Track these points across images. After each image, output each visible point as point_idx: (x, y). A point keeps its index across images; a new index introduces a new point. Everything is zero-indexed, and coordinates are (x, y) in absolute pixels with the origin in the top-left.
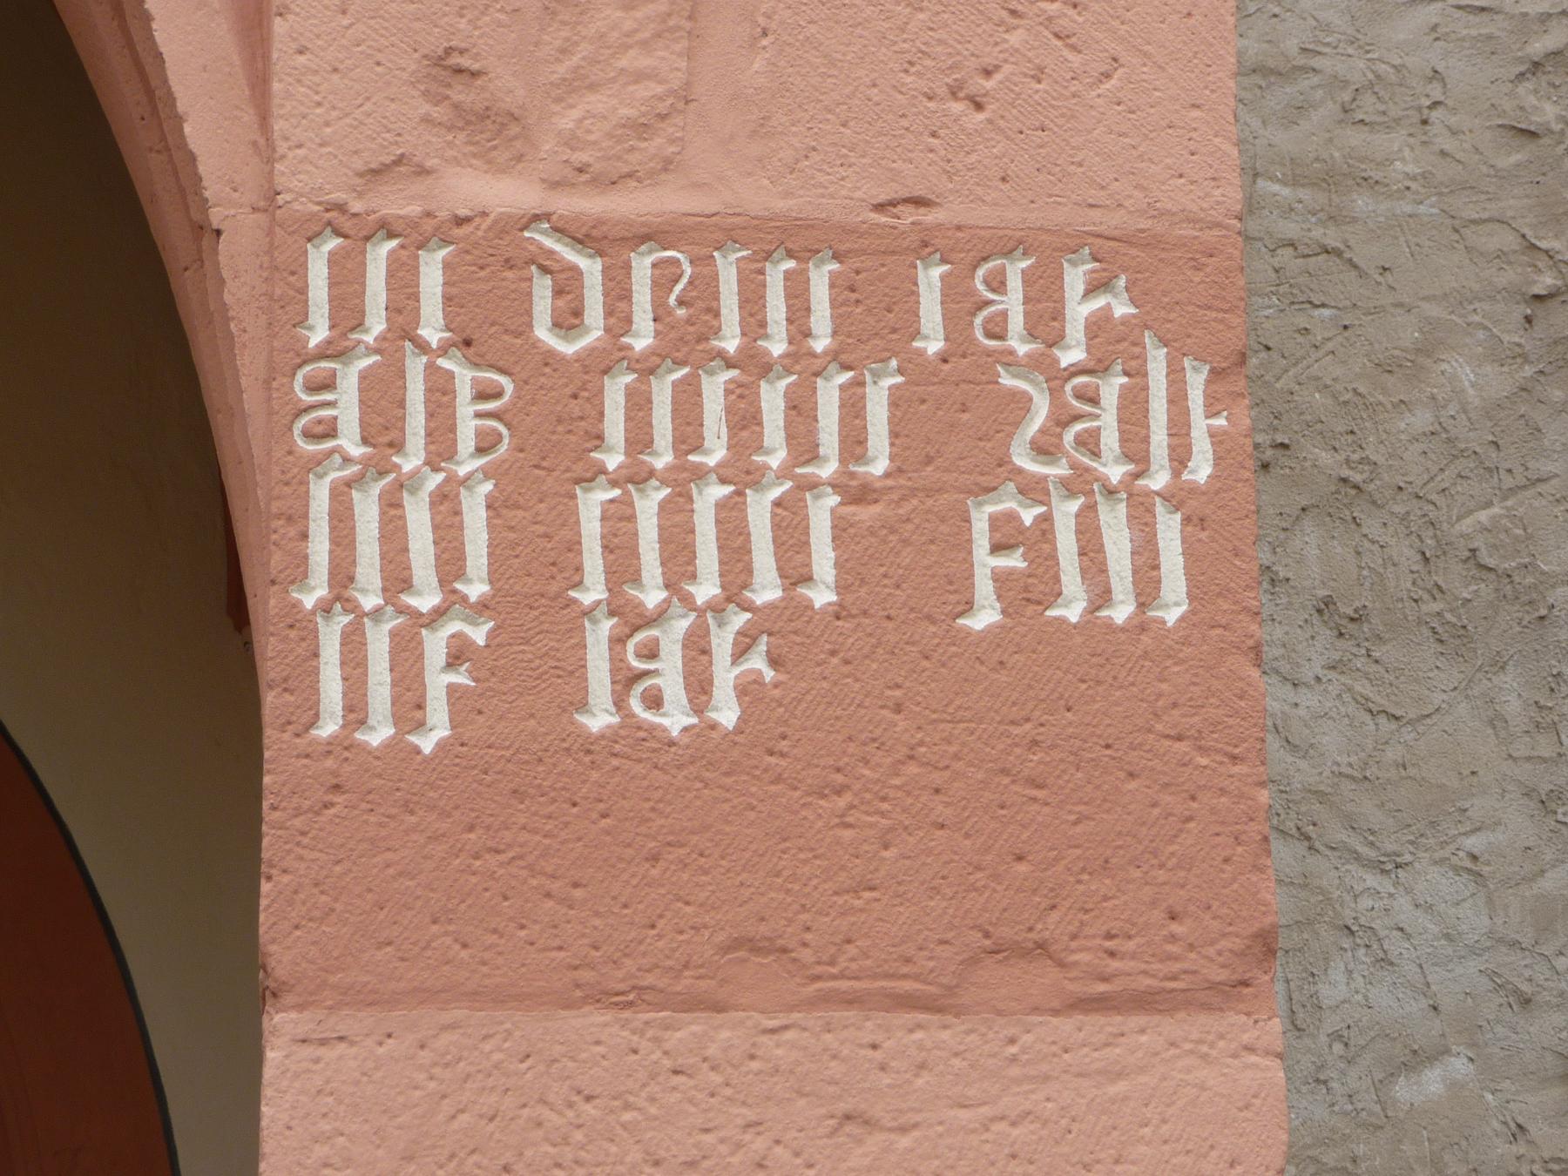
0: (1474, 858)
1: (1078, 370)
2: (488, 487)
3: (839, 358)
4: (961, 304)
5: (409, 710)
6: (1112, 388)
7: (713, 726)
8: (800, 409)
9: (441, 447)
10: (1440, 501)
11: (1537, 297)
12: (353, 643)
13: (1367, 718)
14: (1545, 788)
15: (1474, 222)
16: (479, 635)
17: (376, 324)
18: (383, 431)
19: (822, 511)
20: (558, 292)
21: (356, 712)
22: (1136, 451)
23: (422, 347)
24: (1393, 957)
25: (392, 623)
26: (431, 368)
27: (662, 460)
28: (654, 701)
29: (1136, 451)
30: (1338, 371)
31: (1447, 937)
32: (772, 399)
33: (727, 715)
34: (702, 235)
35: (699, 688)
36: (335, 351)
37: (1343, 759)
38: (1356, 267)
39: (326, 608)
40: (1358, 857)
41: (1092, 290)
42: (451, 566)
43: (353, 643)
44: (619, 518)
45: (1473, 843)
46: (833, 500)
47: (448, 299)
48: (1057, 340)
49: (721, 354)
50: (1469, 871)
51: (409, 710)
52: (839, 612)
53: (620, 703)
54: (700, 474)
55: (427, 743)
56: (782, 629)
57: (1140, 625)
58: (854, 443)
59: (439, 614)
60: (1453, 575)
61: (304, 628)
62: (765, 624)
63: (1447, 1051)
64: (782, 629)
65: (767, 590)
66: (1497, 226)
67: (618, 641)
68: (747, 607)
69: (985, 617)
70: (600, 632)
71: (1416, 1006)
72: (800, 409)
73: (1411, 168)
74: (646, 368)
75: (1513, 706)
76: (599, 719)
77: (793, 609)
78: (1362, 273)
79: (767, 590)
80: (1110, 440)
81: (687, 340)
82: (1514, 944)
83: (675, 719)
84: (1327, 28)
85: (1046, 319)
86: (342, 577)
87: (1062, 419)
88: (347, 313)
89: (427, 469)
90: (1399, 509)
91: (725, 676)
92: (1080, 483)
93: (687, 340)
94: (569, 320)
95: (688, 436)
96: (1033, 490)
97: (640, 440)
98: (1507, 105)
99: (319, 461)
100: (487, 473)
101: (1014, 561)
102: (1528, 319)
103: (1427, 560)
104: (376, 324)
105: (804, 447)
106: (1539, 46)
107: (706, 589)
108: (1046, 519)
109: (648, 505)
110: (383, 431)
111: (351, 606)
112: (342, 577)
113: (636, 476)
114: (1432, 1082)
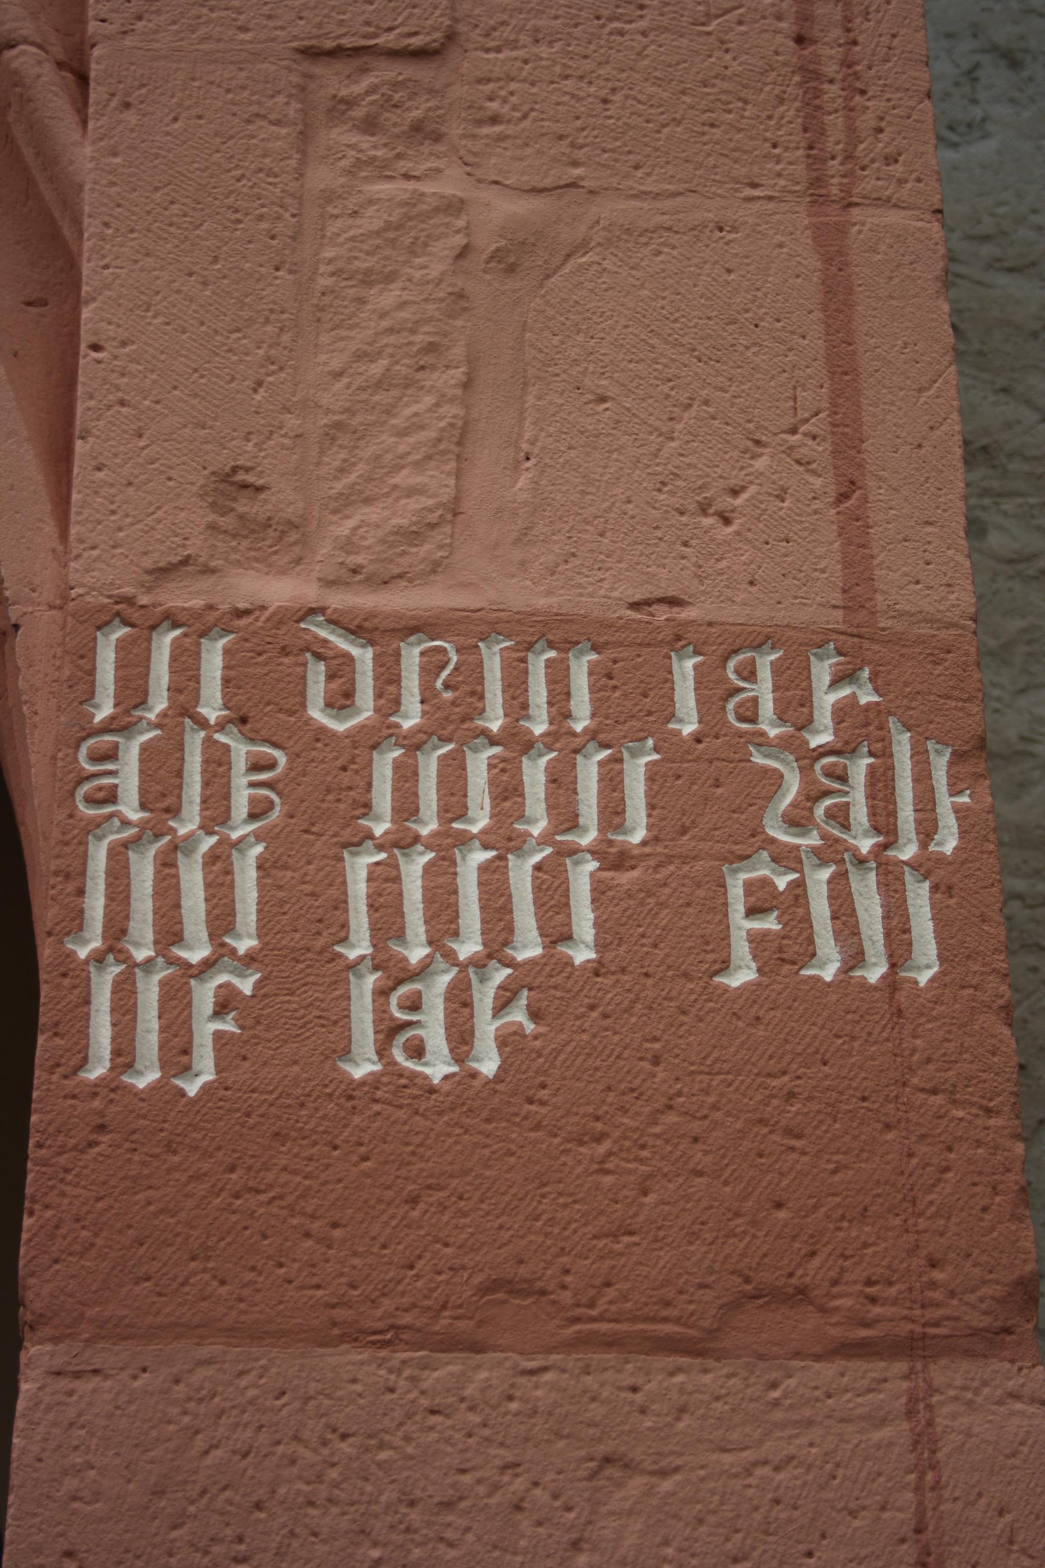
4: (713, 692)
5: (177, 1054)
6: (860, 768)
17: (159, 703)
18: (161, 796)
19: (582, 875)
21: (124, 1055)
22: (884, 823)
23: (202, 723)
26: (209, 743)
28: (417, 1051)
29: (884, 823)
32: (535, 773)
34: (471, 628)
35: (461, 1039)
39: (98, 959)
42: (221, 920)
44: (386, 883)
46: (592, 865)
48: (806, 723)
49: (485, 732)
51: (177, 1054)
52: (597, 969)
53: (382, 1051)
54: (463, 840)
56: (544, 984)
58: (613, 812)
59: (208, 965)
61: (78, 978)
62: (523, 980)
64: (544, 984)
65: (529, 947)
69: (742, 975)
74: (414, 744)
76: (363, 1068)
79: (529, 947)
80: (860, 814)
81: (454, 718)
83: (438, 1068)
85: (796, 706)
86: (117, 930)
87: (812, 795)
88: (133, 692)
91: (487, 1029)
93: (454, 718)
94: (342, 700)
96: (786, 857)
99: (97, 823)
100: (258, 837)
101: (770, 924)
104: (159, 703)
108: (799, 886)
109: (414, 869)
110: (161, 796)
112: (117, 930)
113: (403, 841)
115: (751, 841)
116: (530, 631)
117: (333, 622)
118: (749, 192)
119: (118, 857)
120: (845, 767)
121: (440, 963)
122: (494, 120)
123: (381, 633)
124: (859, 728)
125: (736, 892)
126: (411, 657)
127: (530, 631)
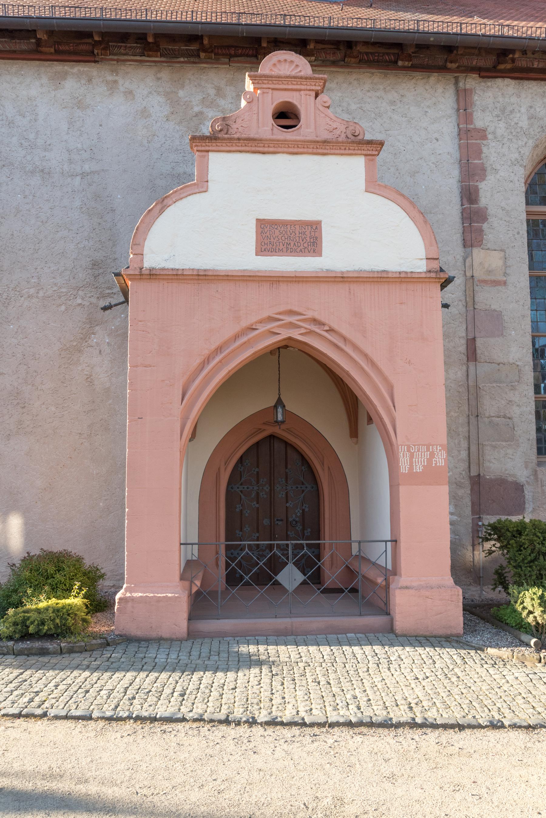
4: (432, 448)
8: (424, 454)
32: (423, 454)
34: (419, 445)
56: (424, 466)
62: (423, 466)
64: (424, 466)
69: (434, 465)
72: (424, 454)
75: (456, 443)
76: (415, 471)
81: (418, 451)
83: (418, 471)
85: (437, 449)
88: (402, 450)
89: (64, 651)
93: (418, 451)
115: (434, 457)
116: (422, 445)
120: (313, 74)
123: (414, 446)
124: (440, 450)
127: (422, 445)
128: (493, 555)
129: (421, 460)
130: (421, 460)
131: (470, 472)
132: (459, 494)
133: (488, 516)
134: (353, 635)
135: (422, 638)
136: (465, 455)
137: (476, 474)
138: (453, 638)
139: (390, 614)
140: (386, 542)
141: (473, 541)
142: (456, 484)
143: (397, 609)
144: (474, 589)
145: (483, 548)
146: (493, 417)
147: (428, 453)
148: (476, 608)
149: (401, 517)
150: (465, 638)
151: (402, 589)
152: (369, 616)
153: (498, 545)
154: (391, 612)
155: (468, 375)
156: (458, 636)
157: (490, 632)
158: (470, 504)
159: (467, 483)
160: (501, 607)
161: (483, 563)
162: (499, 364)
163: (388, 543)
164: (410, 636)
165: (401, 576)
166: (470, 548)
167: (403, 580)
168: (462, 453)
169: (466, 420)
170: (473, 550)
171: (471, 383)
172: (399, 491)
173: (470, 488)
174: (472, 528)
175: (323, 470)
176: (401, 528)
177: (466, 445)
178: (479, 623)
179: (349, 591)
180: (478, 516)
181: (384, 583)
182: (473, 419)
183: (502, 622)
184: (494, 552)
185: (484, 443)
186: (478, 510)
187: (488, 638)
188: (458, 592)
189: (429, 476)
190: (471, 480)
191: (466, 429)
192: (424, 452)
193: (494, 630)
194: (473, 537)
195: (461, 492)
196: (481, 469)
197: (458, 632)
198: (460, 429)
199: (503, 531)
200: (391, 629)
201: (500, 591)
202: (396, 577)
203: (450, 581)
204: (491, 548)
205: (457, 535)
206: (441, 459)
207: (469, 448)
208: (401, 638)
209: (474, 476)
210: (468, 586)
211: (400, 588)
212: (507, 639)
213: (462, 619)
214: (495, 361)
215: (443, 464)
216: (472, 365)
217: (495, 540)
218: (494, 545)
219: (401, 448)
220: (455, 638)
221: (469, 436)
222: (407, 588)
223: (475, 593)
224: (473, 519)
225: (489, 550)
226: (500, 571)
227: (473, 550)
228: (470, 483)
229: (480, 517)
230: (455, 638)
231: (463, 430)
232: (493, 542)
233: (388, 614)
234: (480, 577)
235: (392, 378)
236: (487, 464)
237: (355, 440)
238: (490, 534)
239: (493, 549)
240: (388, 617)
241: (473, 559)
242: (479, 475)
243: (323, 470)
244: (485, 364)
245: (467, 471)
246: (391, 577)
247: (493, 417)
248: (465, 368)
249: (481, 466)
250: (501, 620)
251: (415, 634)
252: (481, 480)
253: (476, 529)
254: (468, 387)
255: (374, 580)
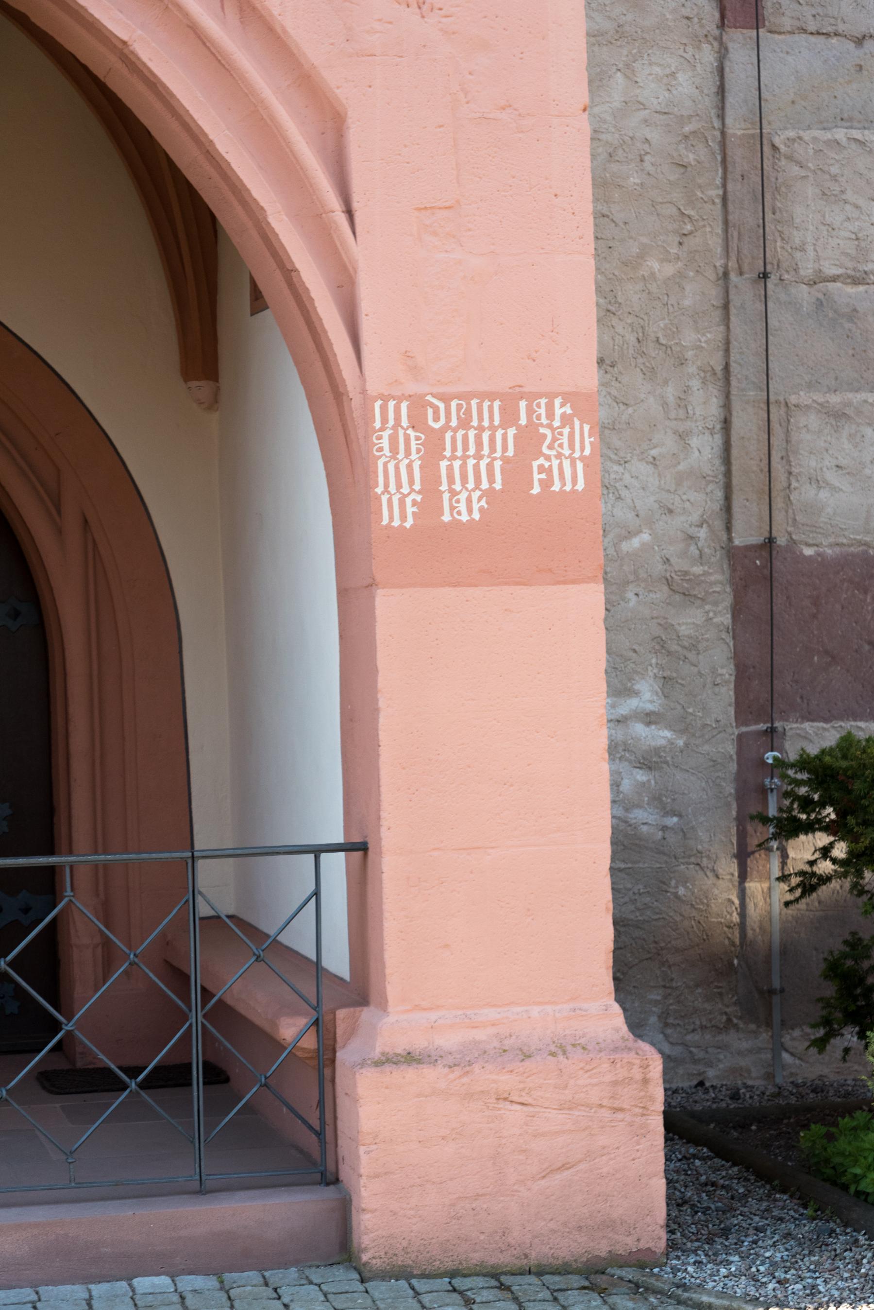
0: (654, 458)
1: (558, 428)
2: (420, 462)
3: (500, 426)
4: (530, 411)
5: (403, 517)
6: (566, 431)
7: (474, 520)
8: (492, 440)
9: (408, 453)
10: (646, 318)
11: (685, 235)
12: (390, 501)
13: (615, 404)
14: (681, 430)
15: (661, 203)
16: (419, 498)
17: (391, 422)
18: (394, 450)
19: (498, 464)
20: (434, 413)
21: (391, 518)
22: (572, 446)
23: (402, 428)
24: (623, 496)
25: (398, 496)
26: (405, 434)
27: (459, 453)
28: (459, 513)
29: (572, 446)
30: (607, 266)
31: (643, 489)
32: (485, 436)
33: (476, 516)
34: (466, 397)
35: (470, 511)
36: (383, 429)
37: (606, 421)
38: (614, 222)
39: (383, 493)
40: (610, 459)
41: (562, 405)
42: (411, 482)
43: (390, 501)
44: (450, 468)
45: (654, 452)
46: (501, 463)
47: (409, 416)
48: (553, 420)
49: (473, 427)
50: (652, 463)
51: (403, 517)
52: (502, 491)
53: (452, 515)
54: (469, 457)
55: (408, 525)
56: (489, 494)
57: (573, 491)
58: (505, 448)
59: (409, 494)
60: (651, 350)
61: (378, 498)
62: (485, 494)
63: (641, 532)
64: (489, 494)
65: (485, 485)
66: (669, 205)
67: (450, 500)
68: (481, 490)
69: (536, 490)
70: (446, 496)
71: (631, 515)
72: (492, 440)
73: (638, 181)
74: (455, 430)
75: (671, 399)
76: (447, 518)
77: (491, 490)
78: (617, 225)
79: (485, 485)
80: (566, 445)
81: (465, 423)
82: (669, 491)
83: (465, 518)
84: (605, 122)
85: (550, 415)
86: (386, 485)
87: (554, 440)
88: (384, 420)
90: (629, 321)
91: (475, 507)
92: (559, 456)
93: (465, 423)
94: (436, 419)
95: (466, 448)
96: (548, 458)
97: (454, 449)
98: (675, 154)
99: (380, 457)
100: (419, 458)
101: (543, 476)
102: (680, 243)
103: (639, 342)
104: (391, 422)
105: (493, 449)
106: (687, 129)
107: (471, 485)
108: (551, 466)
109: (457, 464)
110: (394, 450)
111: (389, 493)
112: (386, 485)
113: (453, 458)
114: (636, 542)
116: (482, 396)
117: (434, 396)
118: (542, 251)
119: (385, 465)
121: (464, 490)
122: (470, 230)
123: (446, 399)
124: (566, 420)
125: (535, 469)
126: (454, 404)
127: (482, 396)
128: (824, 891)
129: (476, 467)
130: (476, 467)
131: (729, 529)
132: (684, 630)
133: (807, 725)
134: (163, 1281)
135: (480, 1282)
136: (707, 453)
137: (756, 539)
138: (618, 1272)
139: (336, 1181)
140: (317, 851)
141: (742, 835)
142: (669, 582)
143: (364, 1159)
144: (745, 1045)
145: (784, 864)
146: (834, 279)
147: (512, 432)
148: (743, 1126)
149: (382, 735)
150: (675, 1270)
151: (387, 1068)
152: (241, 1194)
153: (840, 851)
154: (345, 1173)
155: (722, 91)
156: (642, 1261)
157: (788, 1235)
158: (728, 672)
159: (717, 578)
160: (845, 1122)
161: (783, 930)
162: (859, 41)
163: (324, 856)
164: (424, 1276)
165: (383, 1006)
166: (729, 867)
167: (394, 1024)
168: (695, 442)
169: (714, 294)
170: (743, 876)
171: (736, 127)
172: (373, 608)
173: (727, 600)
174: (740, 779)
175: (60, 532)
176: (383, 789)
177: (714, 409)
178: (745, 1196)
179: (144, 1086)
180: (762, 726)
181: (309, 1042)
182: (744, 292)
183: (845, 1188)
184: (825, 880)
185: (793, 399)
186: (761, 696)
187: (774, 1265)
188: (645, 1067)
189: (510, 544)
190: (733, 569)
191: (714, 334)
192: (493, 428)
193: (808, 1227)
194: (740, 821)
195: (688, 621)
196: (779, 517)
197: (643, 1245)
198: (689, 337)
199: (858, 786)
200: (341, 1248)
201: (847, 1051)
202: (366, 1014)
203: (608, 1019)
204: (812, 863)
205: (674, 813)
206: (568, 462)
207: (727, 423)
208: (384, 1286)
209: (749, 548)
210: (719, 1030)
211: (378, 1064)
212: (859, 1263)
213: (660, 1185)
214: (841, 28)
215: (580, 486)
216: (739, 41)
217: (829, 828)
218: (825, 852)
219: (384, 409)
220: (629, 1274)
221: (727, 368)
222: (410, 1058)
223: (742, 1060)
224: (740, 737)
225: (802, 873)
226: (849, 963)
227: (743, 876)
228: (732, 582)
229: (772, 731)
230: (629, 1274)
231: (699, 340)
232: (822, 839)
233: (329, 1178)
234: (772, 992)
235: (340, 83)
236: (804, 493)
237: (203, 388)
238: (806, 804)
239: (825, 867)
240: (328, 1193)
241: (743, 914)
242: (770, 541)
243: (60, 532)
244: (801, 39)
245: (719, 524)
246: (341, 1014)
247: (834, 279)
248: (708, 55)
249: (779, 503)
250: (838, 1181)
251: (450, 1265)
252: (777, 564)
253: (752, 777)
254: (723, 145)
255: (267, 1027)
